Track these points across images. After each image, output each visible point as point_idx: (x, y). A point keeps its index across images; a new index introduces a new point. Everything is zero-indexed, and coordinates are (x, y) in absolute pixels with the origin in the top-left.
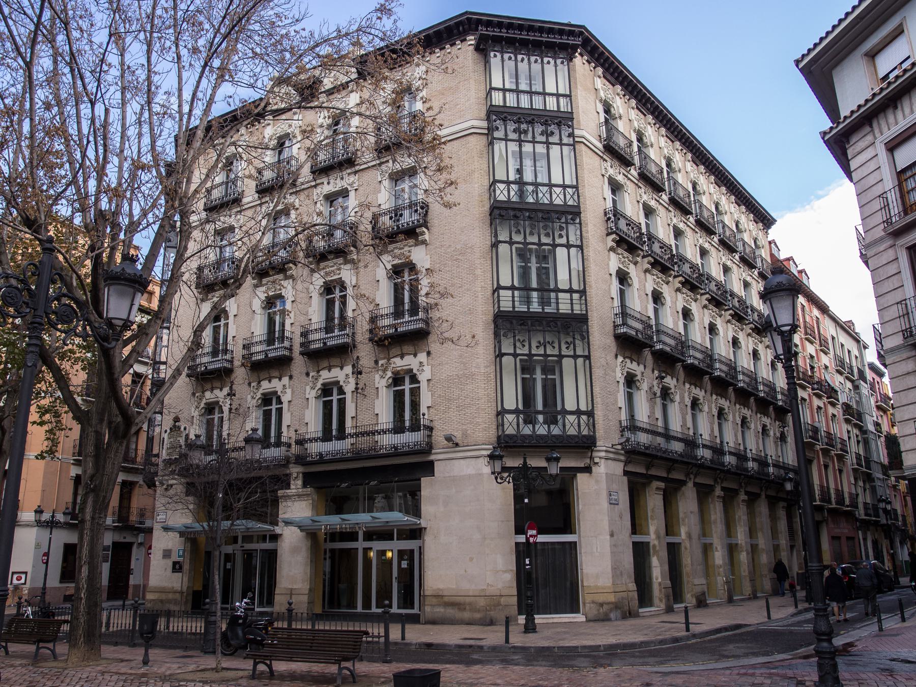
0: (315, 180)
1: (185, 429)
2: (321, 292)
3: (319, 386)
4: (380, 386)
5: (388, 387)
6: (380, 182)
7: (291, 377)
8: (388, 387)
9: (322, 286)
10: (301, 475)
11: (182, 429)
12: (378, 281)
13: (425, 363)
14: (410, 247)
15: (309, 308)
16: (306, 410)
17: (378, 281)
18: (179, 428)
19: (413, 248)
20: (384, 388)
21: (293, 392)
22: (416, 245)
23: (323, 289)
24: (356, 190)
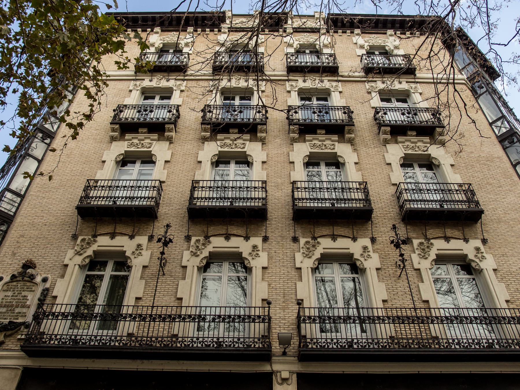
0: (288, 77)
1: (45, 280)
2: (118, 159)
3: (89, 252)
4: (189, 265)
5: (81, 267)
6: (131, 91)
7: (265, 239)
8: (81, 267)
9: (122, 154)
10: (295, 376)
11: (38, 279)
12: (104, 162)
13: (144, 247)
14: (152, 140)
15: (99, 171)
16: (181, 282)
17: (104, 162)
18: (32, 277)
19: (155, 142)
20: (77, 267)
21: (270, 258)
22: (159, 140)
23: (122, 157)
24: (182, 91)
